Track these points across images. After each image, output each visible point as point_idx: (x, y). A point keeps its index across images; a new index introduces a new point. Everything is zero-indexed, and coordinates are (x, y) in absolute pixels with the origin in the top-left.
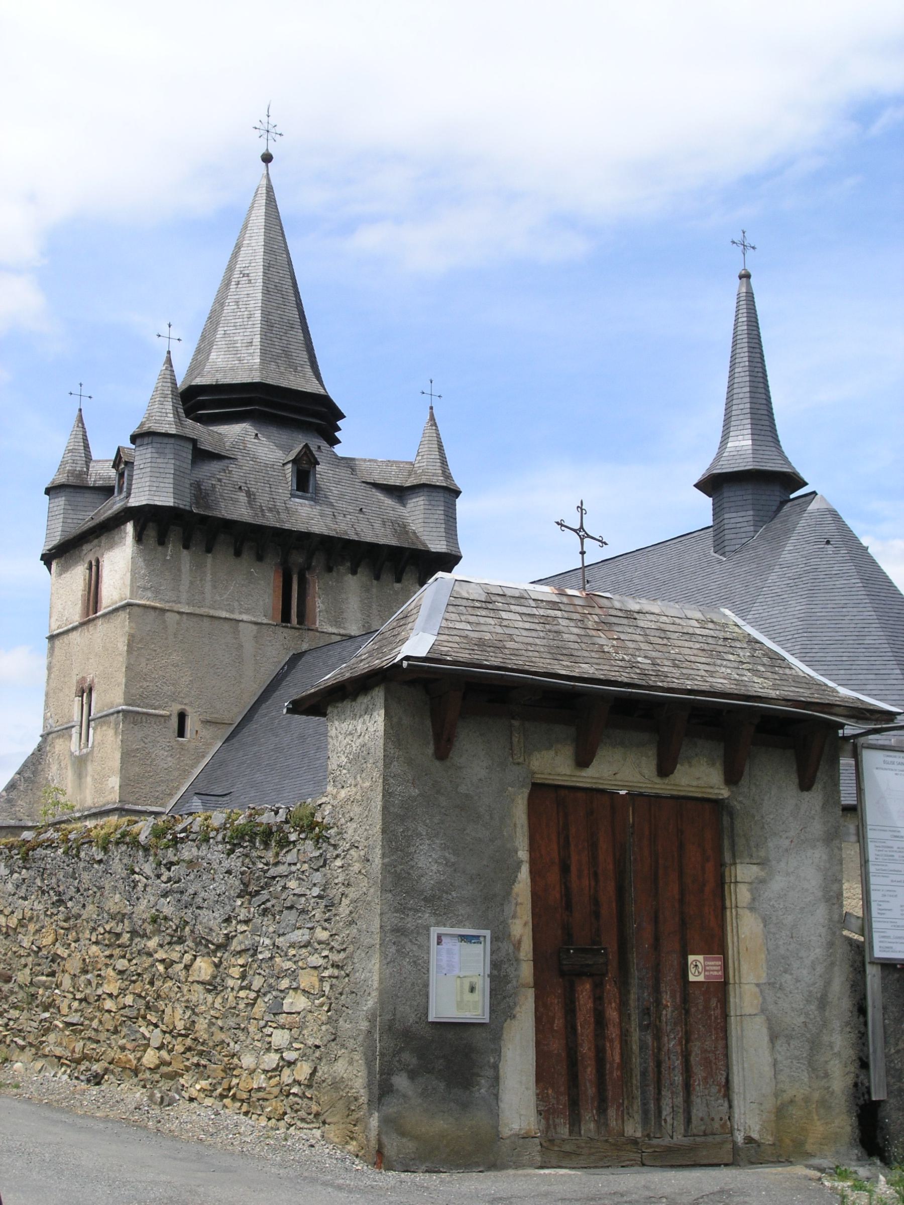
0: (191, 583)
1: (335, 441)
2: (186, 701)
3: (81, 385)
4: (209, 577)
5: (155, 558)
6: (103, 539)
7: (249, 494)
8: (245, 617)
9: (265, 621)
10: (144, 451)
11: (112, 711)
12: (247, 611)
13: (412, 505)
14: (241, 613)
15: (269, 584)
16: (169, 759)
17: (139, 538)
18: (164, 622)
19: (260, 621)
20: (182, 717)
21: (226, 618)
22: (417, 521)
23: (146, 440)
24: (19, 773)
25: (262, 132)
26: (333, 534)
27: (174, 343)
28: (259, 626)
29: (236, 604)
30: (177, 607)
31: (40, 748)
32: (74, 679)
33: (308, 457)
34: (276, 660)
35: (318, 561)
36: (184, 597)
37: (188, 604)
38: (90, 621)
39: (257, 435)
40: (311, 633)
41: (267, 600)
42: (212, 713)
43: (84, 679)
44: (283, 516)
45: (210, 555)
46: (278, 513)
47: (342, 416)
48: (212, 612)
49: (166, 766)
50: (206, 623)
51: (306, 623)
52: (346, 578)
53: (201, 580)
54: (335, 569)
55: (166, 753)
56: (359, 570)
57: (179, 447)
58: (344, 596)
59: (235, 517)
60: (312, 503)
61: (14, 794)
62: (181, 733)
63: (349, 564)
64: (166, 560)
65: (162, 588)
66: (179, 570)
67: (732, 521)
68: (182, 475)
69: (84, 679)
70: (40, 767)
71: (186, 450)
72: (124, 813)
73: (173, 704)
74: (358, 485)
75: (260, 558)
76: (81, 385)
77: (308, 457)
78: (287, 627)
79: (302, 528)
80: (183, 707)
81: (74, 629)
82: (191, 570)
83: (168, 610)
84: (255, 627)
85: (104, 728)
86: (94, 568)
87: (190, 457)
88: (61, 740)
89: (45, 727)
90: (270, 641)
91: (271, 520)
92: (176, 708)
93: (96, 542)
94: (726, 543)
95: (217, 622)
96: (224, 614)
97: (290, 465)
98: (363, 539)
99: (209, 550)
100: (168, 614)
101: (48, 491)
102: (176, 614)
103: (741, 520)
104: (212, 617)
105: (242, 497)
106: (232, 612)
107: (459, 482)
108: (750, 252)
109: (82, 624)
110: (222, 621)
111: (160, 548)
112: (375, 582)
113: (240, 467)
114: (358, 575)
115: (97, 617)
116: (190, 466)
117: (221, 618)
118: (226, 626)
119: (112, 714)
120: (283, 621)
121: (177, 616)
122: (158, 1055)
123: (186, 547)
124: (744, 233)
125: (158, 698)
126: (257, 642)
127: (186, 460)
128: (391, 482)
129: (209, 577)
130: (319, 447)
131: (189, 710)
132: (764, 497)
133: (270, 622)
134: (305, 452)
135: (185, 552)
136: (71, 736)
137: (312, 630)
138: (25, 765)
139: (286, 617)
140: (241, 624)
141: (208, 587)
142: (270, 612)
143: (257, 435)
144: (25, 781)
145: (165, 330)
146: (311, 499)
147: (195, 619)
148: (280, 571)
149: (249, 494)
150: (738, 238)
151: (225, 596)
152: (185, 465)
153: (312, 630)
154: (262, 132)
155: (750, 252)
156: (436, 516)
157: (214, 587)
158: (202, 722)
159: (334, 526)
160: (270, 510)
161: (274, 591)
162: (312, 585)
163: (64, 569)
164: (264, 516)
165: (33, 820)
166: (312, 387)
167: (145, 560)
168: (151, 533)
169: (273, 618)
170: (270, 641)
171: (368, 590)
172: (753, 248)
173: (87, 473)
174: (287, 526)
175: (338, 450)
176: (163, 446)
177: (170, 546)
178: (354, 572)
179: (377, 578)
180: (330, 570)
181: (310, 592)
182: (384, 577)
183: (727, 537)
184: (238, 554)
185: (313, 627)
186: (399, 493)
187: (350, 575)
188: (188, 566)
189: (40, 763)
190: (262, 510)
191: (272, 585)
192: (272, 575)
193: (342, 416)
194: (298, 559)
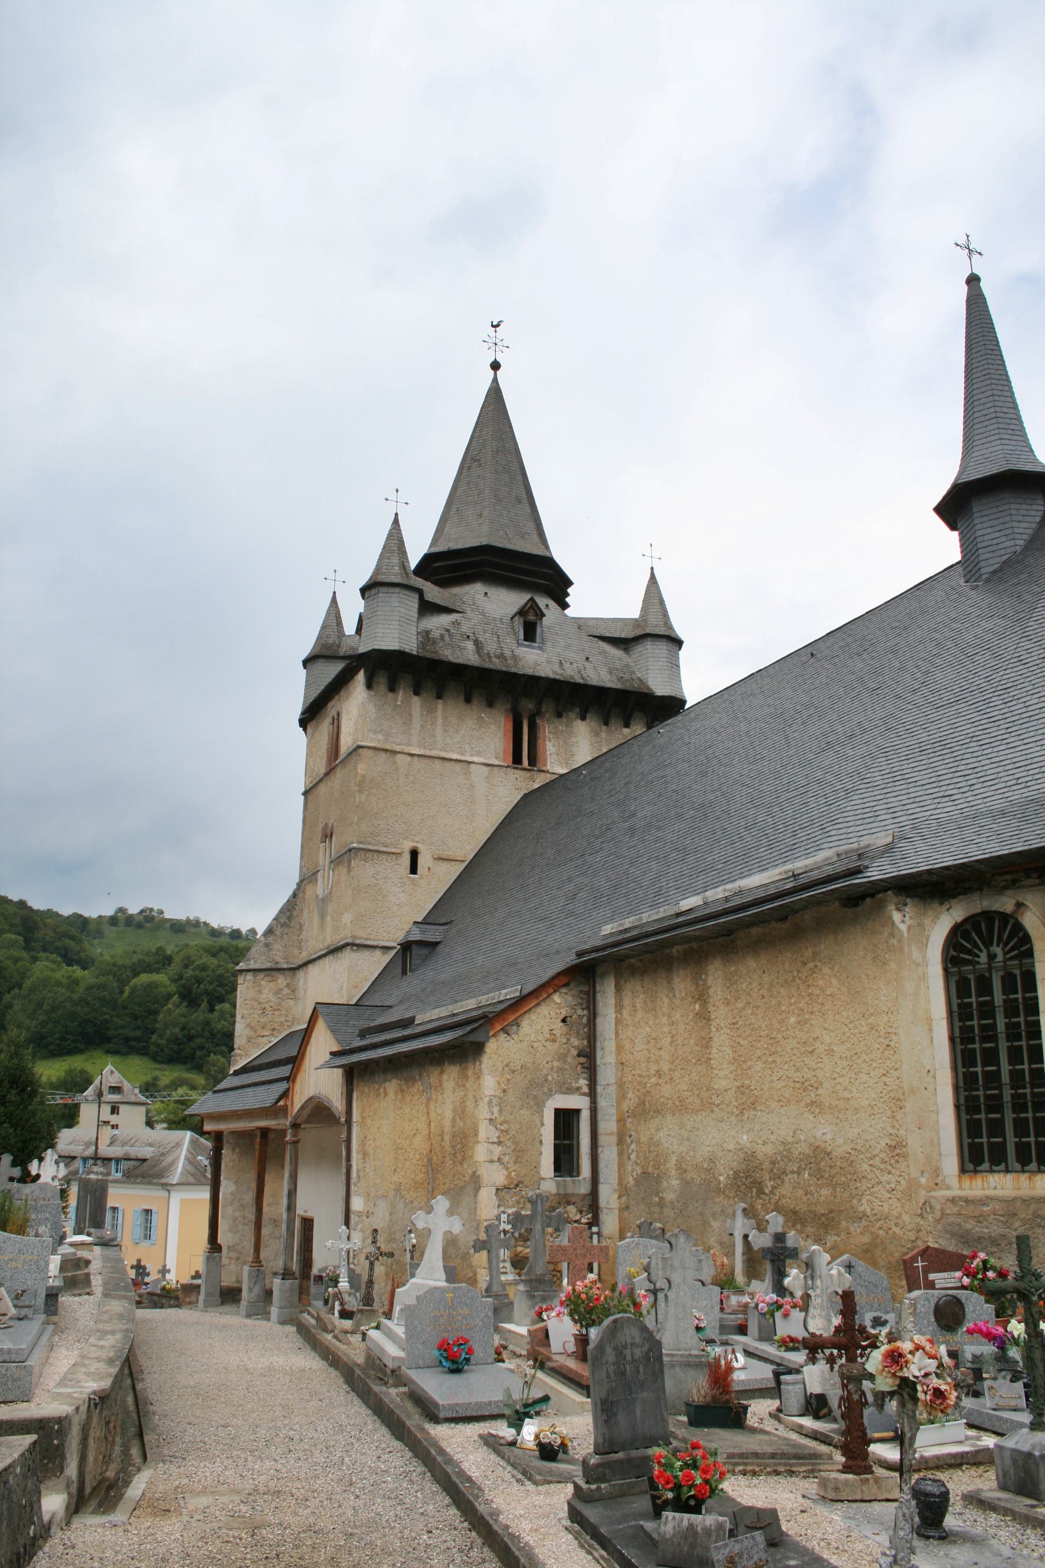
0: (422, 727)
1: (564, 606)
2: (417, 839)
3: (335, 571)
4: (440, 721)
5: (385, 703)
6: (342, 693)
7: (477, 642)
8: (476, 759)
9: (496, 762)
10: (371, 602)
11: (345, 850)
12: (478, 754)
13: (637, 655)
14: (472, 755)
15: (499, 728)
16: (401, 895)
17: (369, 685)
18: (395, 763)
19: (491, 762)
20: (414, 854)
21: (457, 761)
22: (642, 669)
23: (374, 591)
24: (275, 919)
25: (490, 345)
26: (558, 677)
27: (401, 506)
28: (490, 768)
29: (467, 747)
30: (407, 749)
31: (295, 895)
32: (321, 826)
33: (534, 610)
34: (507, 799)
35: (548, 707)
36: (415, 739)
37: (419, 746)
38: (331, 770)
39: (486, 593)
40: (542, 775)
41: (498, 744)
42: (444, 850)
43: (327, 824)
44: (510, 662)
45: (440, 701)
46: (506, 660)
47: (569, 583)
48: (443, 754)
49: (398, 902)
50: (438, 764)
51: (538, 765)
52: (575, 723)
53: (432, 724)
54: (564, 714)
55: (398, 889)
56: (588, 716)
57: (404, 596)
58: (573, 739)
59: (461, 661)
60: (540, 652)
61: (270, 939)
62: (414, 870)
63: (578, 710)
64: (396, 706)
65: (393, 731)
66: (410, 715)
67: (986, 538)
68: (408, 622)
69: (327, 824)
70: (295, 913)
71: (412, 599)
72: (355, 948)
73: (405, 841)
74: (585, 638)
75: (490, 704)
76: (335, 571)
77: (534, 610)
78: (517, 768)
79: (529, 672)
80: (415, 844)
81: (321, 780)
82: (422, 715)
83: (399, 752)
84: (486, 769)
85: (340, 868)
86: (336, 721)
87: (416, 606)
88: (310, 885)
89: (300, 876)
90: (502, 782)
91: (497, 664)
92: (408, 846)
93: (337, 697)
94: (982, 564)
95: (448, 764)
96: (455, 756)
97: (517, 618)
98: (590, 683)
99: (439, 697)
100: (399, 756)
101: (306, 663)
102: (407, 756)
103: (998, 534)
104: (443, 759)
105: (470, 645)
106: (463, 754)
107: (680, 632)
108: (975, 257)
109: (327, 774)
110: (453, 762)
111: (390, 695)
112: (604, 727)
113: (469, 620)
114: (588, 720)
115: (337, 765)
116: (416, 615)
117: (450, 760)
118: (458, 767)
119: (346, 853)
120: (514, 762)
121: (409, 758)
122: (8, 1284)
123: (417, 693)
124: (968, 236)
125: (389, 836)
126: (488, 782)
127: (412, 609)
128: (617, 635)
129: (440, 721)
130: (547, 606)
131: (421, 848)
132: (1024, 507)
133: (502, 764)
134: (531, 606)
135: (416, 699)
136: (317, 881)
137: (543, 771)
138: (281, 911)
139: (517, 759)
140: (472, 765)
141: (439, 730)
142: (501, 754)
143: (486, 593)
144: (282, 926)
145: (392, 496)
146: (540, 648)
147: (426, 761)
148: (511, 716)
149: (477, 642)
150: (962, 241)
151: (456, 739)
152: (411, 613)
153: (543, 771)
154: (490, 345)
155: (975, 257)
156: (661, 664)
157: (445, 731)
158: (435, 859)
159: (560, 671)
160: (498, 657)
161: (505, 735)
162: (541, 729)
163: (316, 728)
164: (491, 661)
165: (287, 963)
166: (537, 551)
167: (375, 705)
168: (382, 681)
169: (504, 761)
170: (502, 782)
171: (597, 734)
172: (980, 254)
173: (339, 646)
174: (513, 670)
175: (567, 612)
176: (388, 595)
177: (401, 693)
178: (583, 718)
179: (606, 723)
180: (559, 715)
181: (540, 735)
182: (612, 722)
183: (981, 557)
184: (468, 700)
185: (544, 769)
186: (623, 643)
187: (579, 721)
188: (418, 710)
189: (295, 909)
190: (490, 657)
191: (502, 729)
192: (503, 719)
193: (569, 583)
194: (528, 705)
